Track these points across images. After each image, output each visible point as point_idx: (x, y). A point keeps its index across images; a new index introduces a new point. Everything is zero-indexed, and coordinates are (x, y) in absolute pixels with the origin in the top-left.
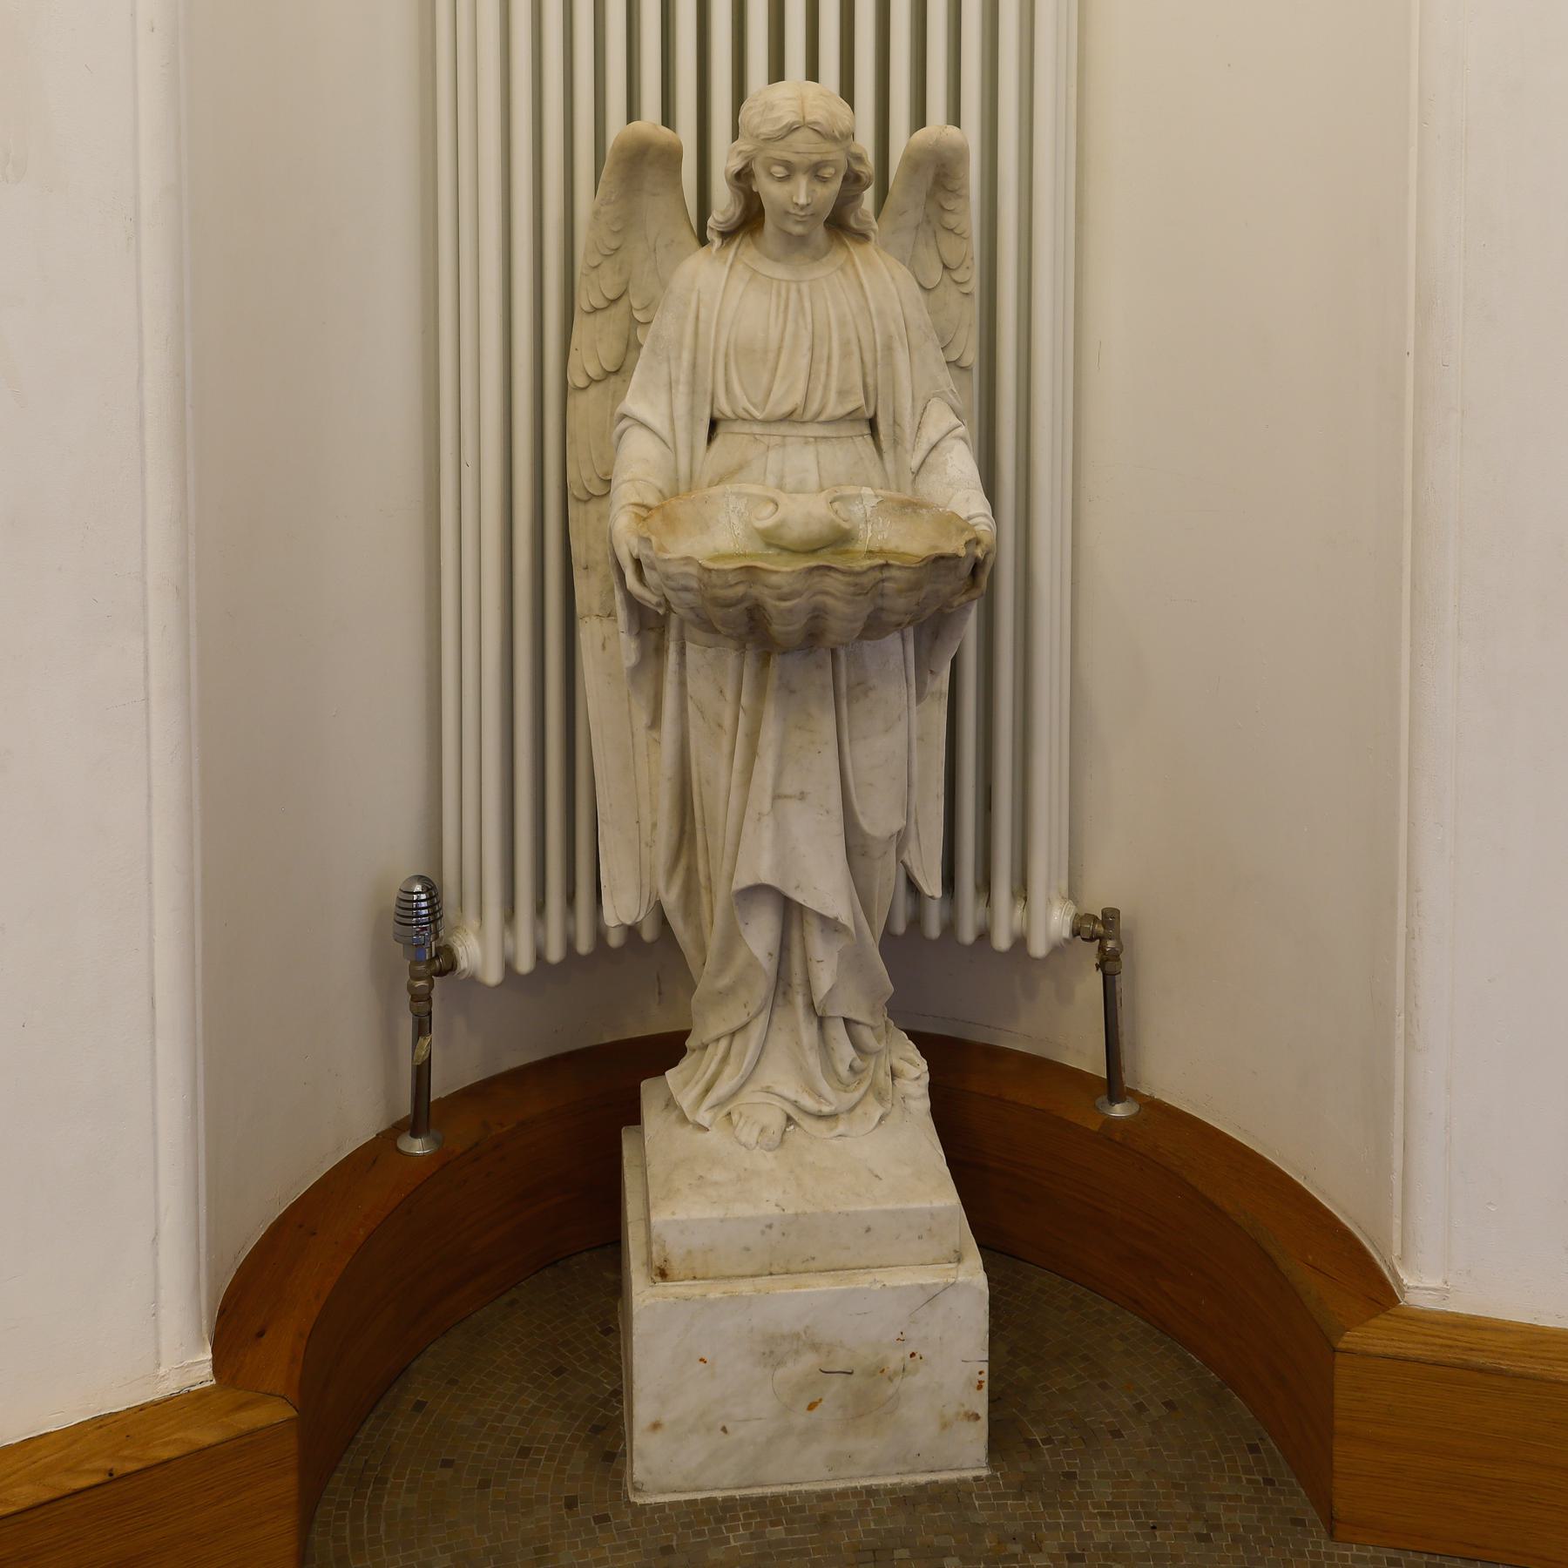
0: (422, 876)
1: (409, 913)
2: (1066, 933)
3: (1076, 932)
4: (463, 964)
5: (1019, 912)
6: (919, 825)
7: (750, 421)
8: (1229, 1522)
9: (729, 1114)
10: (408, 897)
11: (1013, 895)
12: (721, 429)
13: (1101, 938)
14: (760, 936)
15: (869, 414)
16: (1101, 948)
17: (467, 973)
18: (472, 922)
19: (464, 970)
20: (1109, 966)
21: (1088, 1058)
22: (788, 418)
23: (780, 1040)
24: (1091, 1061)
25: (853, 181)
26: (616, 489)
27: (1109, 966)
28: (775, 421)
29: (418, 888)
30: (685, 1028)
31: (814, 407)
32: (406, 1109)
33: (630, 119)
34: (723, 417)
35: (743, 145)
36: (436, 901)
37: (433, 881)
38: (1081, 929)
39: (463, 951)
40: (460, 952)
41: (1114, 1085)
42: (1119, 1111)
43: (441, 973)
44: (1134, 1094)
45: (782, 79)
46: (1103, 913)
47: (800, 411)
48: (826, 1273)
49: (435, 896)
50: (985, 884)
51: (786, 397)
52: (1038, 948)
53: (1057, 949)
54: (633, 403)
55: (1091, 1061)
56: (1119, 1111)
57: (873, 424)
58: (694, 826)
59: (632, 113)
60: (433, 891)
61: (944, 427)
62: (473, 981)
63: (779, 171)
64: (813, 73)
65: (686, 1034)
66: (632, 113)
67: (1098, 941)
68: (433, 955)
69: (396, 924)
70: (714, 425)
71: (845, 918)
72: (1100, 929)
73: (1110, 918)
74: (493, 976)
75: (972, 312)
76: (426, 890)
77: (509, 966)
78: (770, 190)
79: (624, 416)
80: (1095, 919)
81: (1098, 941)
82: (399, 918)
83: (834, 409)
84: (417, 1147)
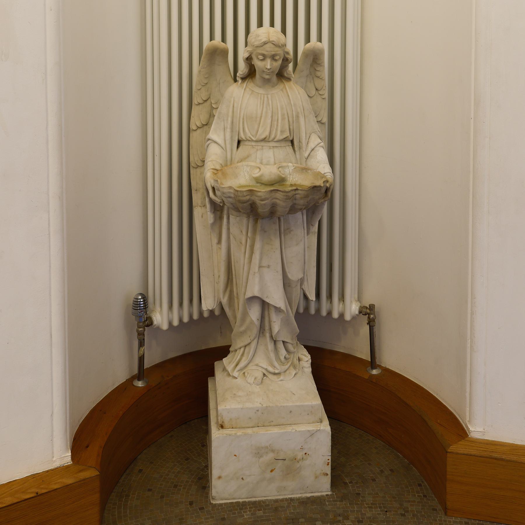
0: (141, 293)
1: (137, 306)
2: (357, 312)
3: (360, 312)
4: (155, 323)
5: (341, 305)
6: (308, 276)
7: (251, 141)
8: (412, 510)
9: (244, 373)
10: (137, 300)
11: (339, 300)
12: (241, 144)
13: (369, 314)
14: (254, 313)
15: (291, 139)
16: (369, 318)
17: (156, 326)
18: (158, 309)
19: (155, 325)
20: (371, 323)
21: (364, 354)
22: (264, 140)
23: (261, 348)
24: (365, 355)
25: (286, 61)
26: (206, 164)
27: (371, 323)
28: (260, 141)
29: (140, 297)
30: (229, 344)
31: (273, 136)
32: (136, 371)
33: (211, 40)
34: (242, 140)
35: (249, 48)
36: (146, 302)
37: (145, 295)
38: (362, 311)
39: (155, 319)
40: (154, 319)
41: (373, 363)
42: (375, 372)
43: (148, 326)
44: (380, 366)
45: (262, 26)
46: (369, 306)
47: (268, 138)
48: (276, 426)
49: (146, 300)
50: (330, 296)
51: (263, 133)
52: (348, 317)
53: (354, 318)
54: (212, 135)
55: (365, 355)
56: (375, 372)
57: (292, 142)
58: (233, 276)
59: (212, 38)
60: (145, 298)
61: (316, 143)
62: (158, 328)
63: (261, 57)
64: (272, 25)
65: (230, 346)
66: (212, 38)
67: (368, 315)
68: (145, 320)
69: (132, 309)
70: (239, 142)
71: (283, 307)
72: (368, 311)
73: (372, 307)
74: (165, 327)
75: (325, 104)
76: (143, 298)
77: (170, 324)
78: (258, 64)
79: (209, 139)
80: (367, 308)
81: (368, 315)
82: (133, 308)
83: (279, 137)
84: (140, 384)
